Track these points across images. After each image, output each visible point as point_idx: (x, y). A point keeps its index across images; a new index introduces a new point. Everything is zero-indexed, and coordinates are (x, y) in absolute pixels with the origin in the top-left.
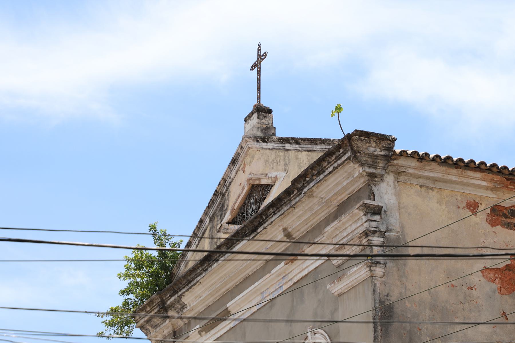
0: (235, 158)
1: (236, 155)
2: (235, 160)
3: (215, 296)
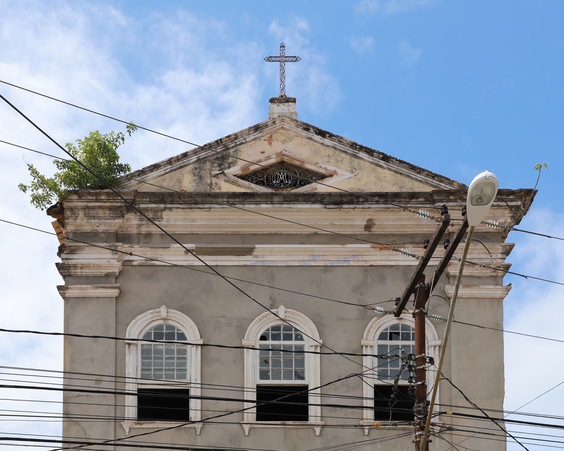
0: (261, 126)
1: (264, 125)
2: (260, 128)
3: (187, 229)
